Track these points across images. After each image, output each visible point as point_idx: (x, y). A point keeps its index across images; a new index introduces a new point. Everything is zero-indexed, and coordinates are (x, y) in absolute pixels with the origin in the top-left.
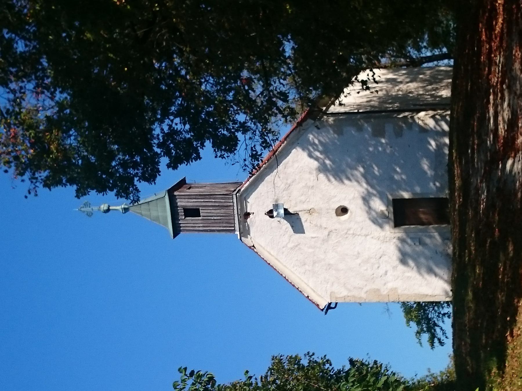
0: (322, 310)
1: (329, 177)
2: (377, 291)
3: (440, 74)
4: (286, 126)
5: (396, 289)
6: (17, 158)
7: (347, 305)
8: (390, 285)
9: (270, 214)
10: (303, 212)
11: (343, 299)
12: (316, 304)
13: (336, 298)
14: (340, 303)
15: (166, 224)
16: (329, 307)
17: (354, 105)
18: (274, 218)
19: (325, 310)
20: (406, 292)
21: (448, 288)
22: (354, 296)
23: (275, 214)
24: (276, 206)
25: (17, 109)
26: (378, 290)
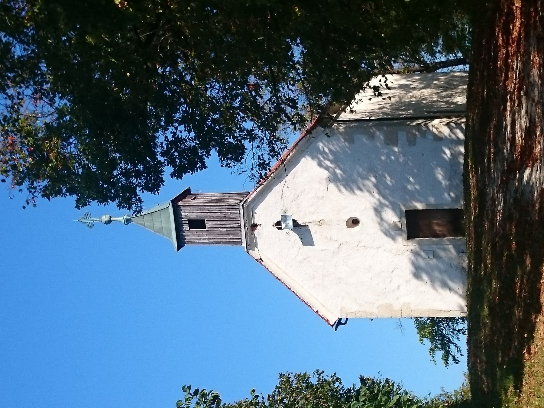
2: (389, 306)
9: (278, 225)
16: (339, 323)
24: (285, 217)
26: (391, 305)
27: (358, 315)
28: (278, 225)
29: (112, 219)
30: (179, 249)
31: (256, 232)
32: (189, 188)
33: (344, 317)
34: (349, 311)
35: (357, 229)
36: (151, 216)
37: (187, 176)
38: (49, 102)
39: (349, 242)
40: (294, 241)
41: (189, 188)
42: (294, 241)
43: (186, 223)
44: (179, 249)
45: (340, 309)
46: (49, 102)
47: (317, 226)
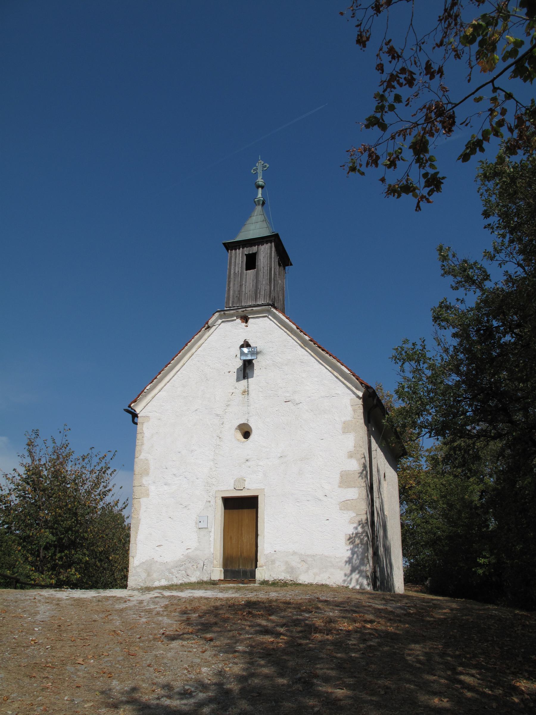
0: (130, 406)
1: (207, 705)
2: (146, 472)
3: (420, 663)
4: (351, 522)
5: (148, 495)
6: (116, 562)
7: (136, 430)
8: (152, 488)
9: (246, 344)
10: (246, 384)
11: (141, 431)
12: (137, 399)
13: (143, 423)
14: (137, 428)
15: (79, 602)
16: (135, 415)
17: (505, 3)
18: (240, 349)
19: (130, 409)
20: (143, 508)
21: (265, 225)
22: (142, 444)
23: (245, 350)
24: (256, 353)
25: (482, 305)
26: (148, 474)
27: (139, 436)
28: (246, 344)
29: (260, 189)
30: (224, 244)
31: (239, 321)
32: (380, 180)
33: (139, 420)
34: (144, 426)
35: (240, 436)
36: (262, 220)
37: (387, 187)
38: (101, 492)
39: (223, 426)
40: (226, 364)
41: (380, 180)
42: (226, 364)
43: (254, 249)
44: (224, 244)
45: (147, 415)
46: (101, 492)
47: (243, 388)
